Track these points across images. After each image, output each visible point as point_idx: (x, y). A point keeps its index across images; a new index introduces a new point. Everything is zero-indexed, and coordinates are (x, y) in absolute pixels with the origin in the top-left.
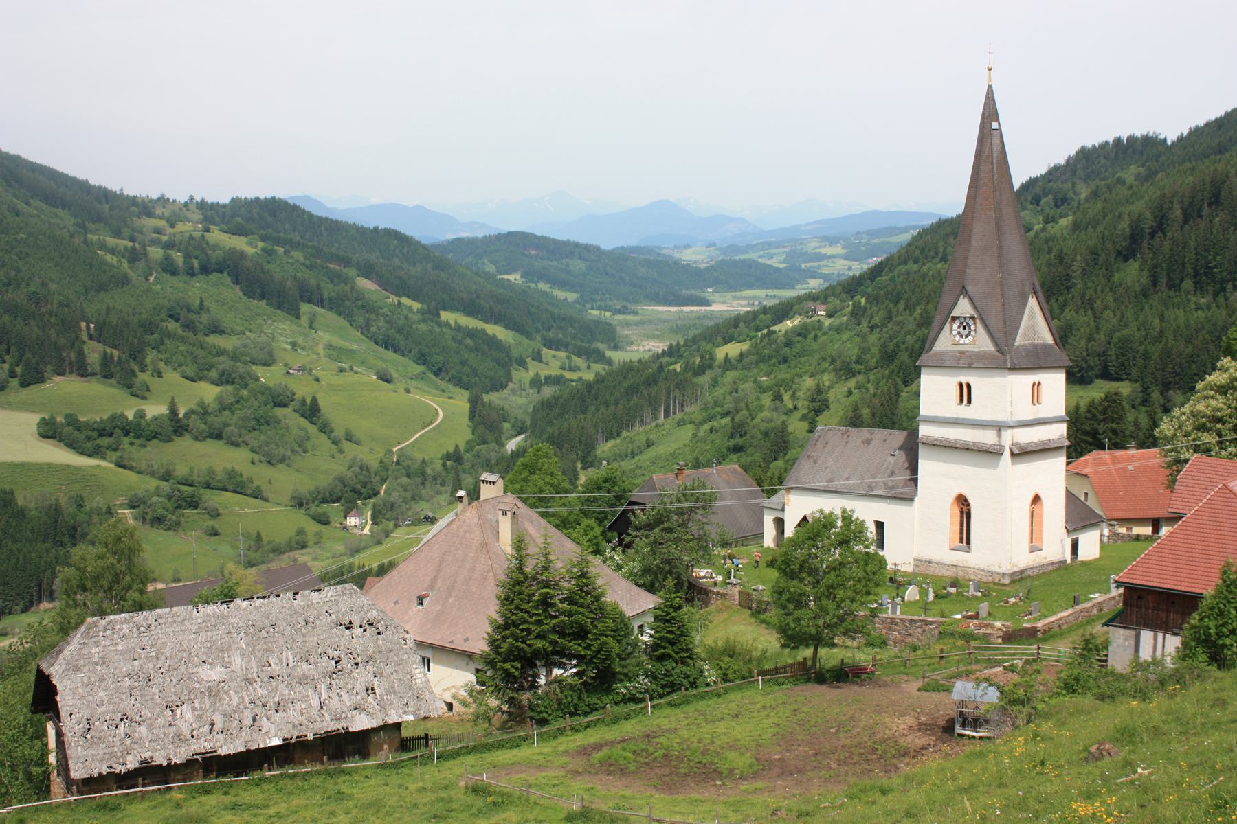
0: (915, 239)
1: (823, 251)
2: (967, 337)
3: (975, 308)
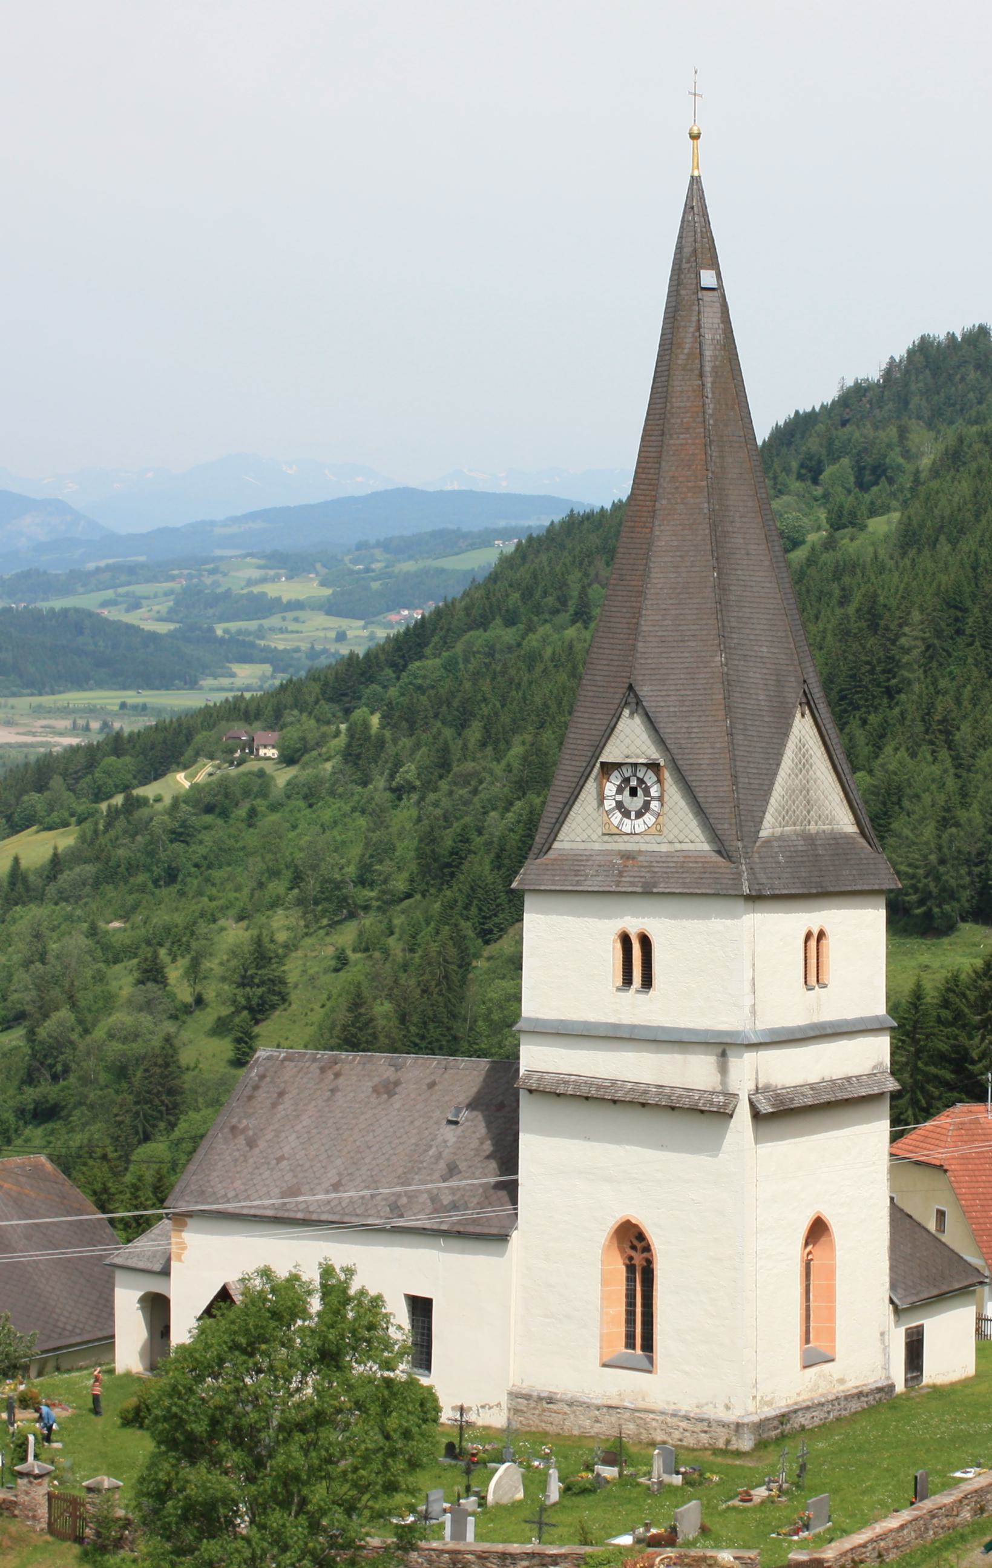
0: (507, 562)
1: (272, 590)
2: (639, 814)
3: (660, 741)
